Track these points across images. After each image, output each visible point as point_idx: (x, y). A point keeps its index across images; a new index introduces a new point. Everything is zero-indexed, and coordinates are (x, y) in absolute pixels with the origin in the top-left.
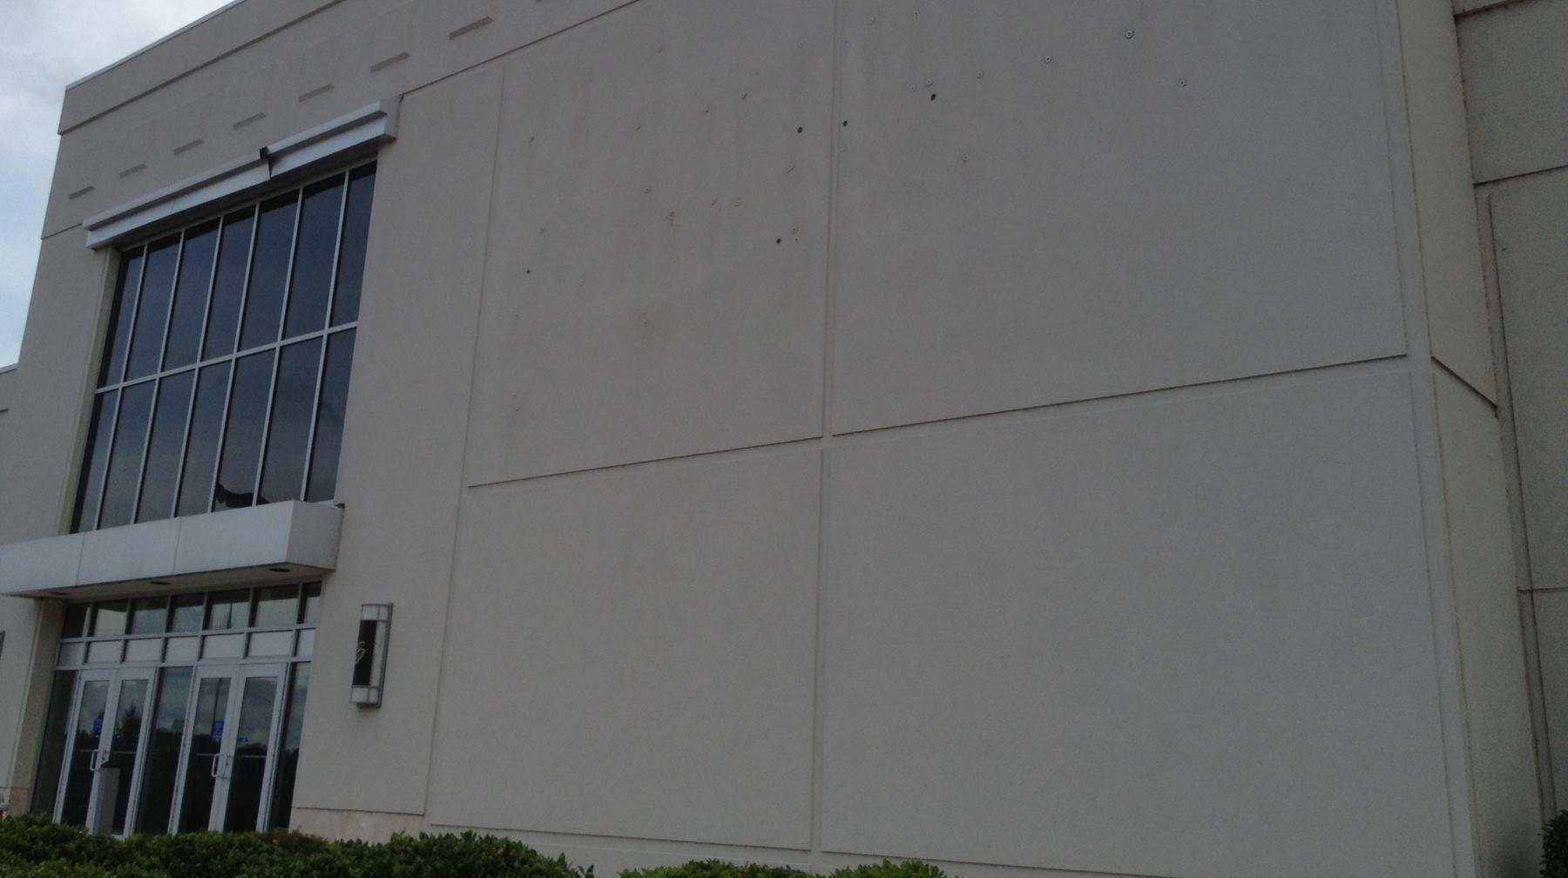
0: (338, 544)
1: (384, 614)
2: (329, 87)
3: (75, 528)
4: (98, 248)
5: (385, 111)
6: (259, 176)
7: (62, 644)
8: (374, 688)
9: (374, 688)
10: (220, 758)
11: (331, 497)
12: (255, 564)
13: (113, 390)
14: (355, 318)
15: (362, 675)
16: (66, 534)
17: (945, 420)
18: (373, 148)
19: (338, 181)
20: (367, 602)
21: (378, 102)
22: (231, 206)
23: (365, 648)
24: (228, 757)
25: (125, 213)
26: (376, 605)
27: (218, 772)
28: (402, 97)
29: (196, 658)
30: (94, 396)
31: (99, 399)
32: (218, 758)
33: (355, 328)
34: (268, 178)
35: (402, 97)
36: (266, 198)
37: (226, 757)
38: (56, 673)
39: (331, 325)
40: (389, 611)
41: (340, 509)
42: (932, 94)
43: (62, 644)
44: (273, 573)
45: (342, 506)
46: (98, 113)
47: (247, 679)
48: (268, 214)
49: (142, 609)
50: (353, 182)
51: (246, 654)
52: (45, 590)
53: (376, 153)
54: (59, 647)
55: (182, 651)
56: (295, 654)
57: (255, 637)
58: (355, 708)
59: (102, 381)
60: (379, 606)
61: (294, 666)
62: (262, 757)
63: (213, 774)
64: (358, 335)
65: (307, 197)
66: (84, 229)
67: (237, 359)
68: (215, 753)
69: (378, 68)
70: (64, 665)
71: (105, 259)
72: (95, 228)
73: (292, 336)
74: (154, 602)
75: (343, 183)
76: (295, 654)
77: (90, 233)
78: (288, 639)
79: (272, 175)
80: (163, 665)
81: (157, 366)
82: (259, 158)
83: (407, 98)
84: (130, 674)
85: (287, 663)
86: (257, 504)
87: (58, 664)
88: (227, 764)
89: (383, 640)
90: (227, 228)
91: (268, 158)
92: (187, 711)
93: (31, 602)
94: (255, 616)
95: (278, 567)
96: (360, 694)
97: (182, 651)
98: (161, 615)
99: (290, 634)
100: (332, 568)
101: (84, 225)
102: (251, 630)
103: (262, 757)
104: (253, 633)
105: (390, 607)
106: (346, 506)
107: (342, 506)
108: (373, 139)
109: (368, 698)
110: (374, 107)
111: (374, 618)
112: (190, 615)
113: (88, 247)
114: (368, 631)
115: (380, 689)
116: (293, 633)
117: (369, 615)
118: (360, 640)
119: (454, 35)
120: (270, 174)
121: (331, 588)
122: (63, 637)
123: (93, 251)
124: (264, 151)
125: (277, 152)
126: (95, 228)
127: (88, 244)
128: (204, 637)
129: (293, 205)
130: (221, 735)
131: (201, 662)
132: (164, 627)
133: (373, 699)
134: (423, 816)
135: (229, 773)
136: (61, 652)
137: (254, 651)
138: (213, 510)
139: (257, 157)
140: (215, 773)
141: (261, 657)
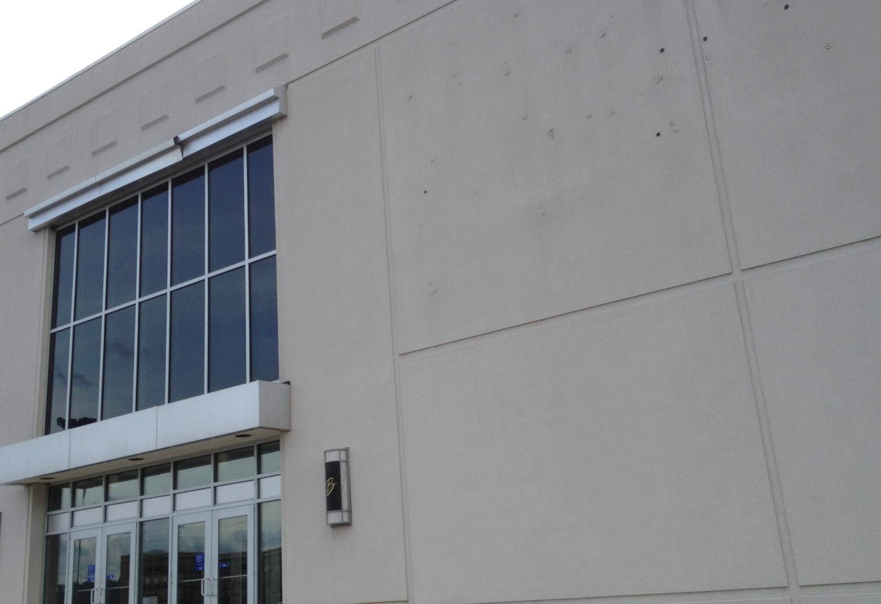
0: (290, 411)
1: (343, 458)
2: (221, 89)
3: (47, 431)
4: (37, 231)
5: (278, 96)
6: (175, 157)
7: (48, 516)
8: (345, 511)
9: (345, 511)
10: (95, 591)
11: (277, 378)
12: (211, 436)
13: (98, 317)
14: (274, 248)
15: (334, 502)
16: (42, 436)
17: (688, 284)
18: (268, 124)
19: (102, 216)
20: (328, 449)
21: (273, 89)
22: (84, 214)
23: (334, 482)
24: (101, 589)
25: (78, 192)
26: (336, 450)
27: (205, 593)
28: (286, 86)
29: (171, 511)
30: (49, 335)
31: (53, 336)
32: (94, 591)
33: (275, 255)
34: (182, 159)
35: (286, 86)
36: (177, 176)
37: (212, 580)
38: (48, 537)
39: (140, 297)
40: (346, 453)
41: (287, 385)
42: (785, 5)
43: (48, 516)
44: (132, 461)
45: (288, 383)
46: (201, 34)
47: (108, 536)
48: (114, 215)
49: (114, 482)
50: (81, 230)
51: (105, 520)
52: (35, 477)
53: (271, 129)
54: (47, 518)
55: (157, 507)
56: (141, 516)
57: (219, 489)
58: (329, 528)
59: (54, 325)
60: (339, 450)
61: (259, 505)
62: (127, 587)
63: (202, 593)
64: (277, 257)
65: (81, 228)
66: (26, 217)
67: (74, 327)
68: (202, 578)
69: (260, 69)
70: (53, 531)
71: (45, 236)
72: (33, 216)
73: (111, 308)
74: (124, 476)
75: (204, 174)
76: (141, 516)
77: (30, 219)
78: (135, 506)
79: (184, 156)
80: (141, 520)
81: (70, 317)
82: (174, 144)
83: (291, 86)
84: (113, 530)
85: (137, 523)
86: (209, 392)
87: (47, 531)
88: (101, 595)
89: (346, 474)
90: (112, 217)
91: (181, 144)
92: (67, 564)
93: (21, 488)
94: (260, 466)
95: (135, 457)
96: (335, 517)
97: (157, 507)
98: (133, 485)
99: (253, 482)
100: (286, 428)
101: (25, 215)
102: (73, 509)
103: (127, 587)
104: (144, 499)
105: (347, 450)
106: (291, 383)
107: (288, 383)
108: (267, 119)
109: (342, 518)
110: (270, 93)
111: (337, 459)
112: (158, 482)
113: (29, 230)
114: (333, 470)
115: (350, 511)
116: (256, 482)
117: (332, 457)
118: (327, 478)
119: (325, 35)
120: (183, 156)
121: (287, 444)
122: (48, 511)
123: (34, 233)
124: (176, 139)
125: (186, 139)
126: (33, 216)
127: (29, 229)
128: (174, 495)
129: (103, 220)
130: (94, 574)
131: (175, 514)
132: (212, 480)
133: (346, 520)
134: (407, 601)
135: (215, 591)
136: (48, 522)
137: (220, 500)
138: (169, 402)
139: (172, 143)
140: (204, 593)
141: (114, 521)
